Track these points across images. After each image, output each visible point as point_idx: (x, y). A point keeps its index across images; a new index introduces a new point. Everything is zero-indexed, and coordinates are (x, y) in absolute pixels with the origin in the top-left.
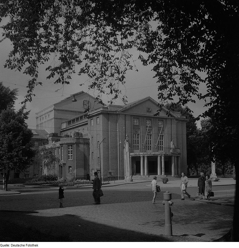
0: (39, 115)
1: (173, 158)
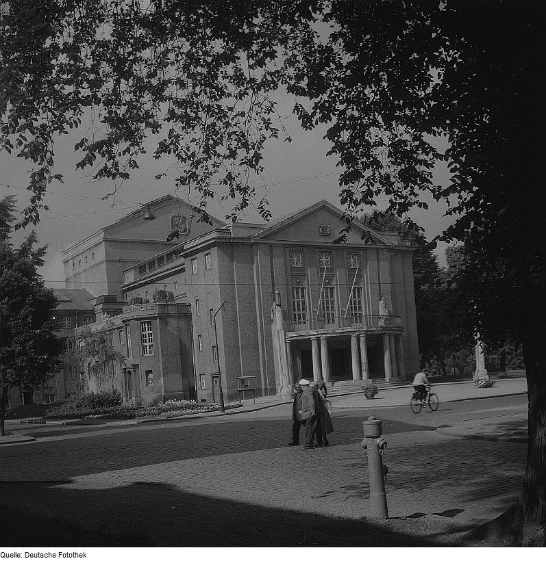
0: (70, 255)
1: (387, 338)
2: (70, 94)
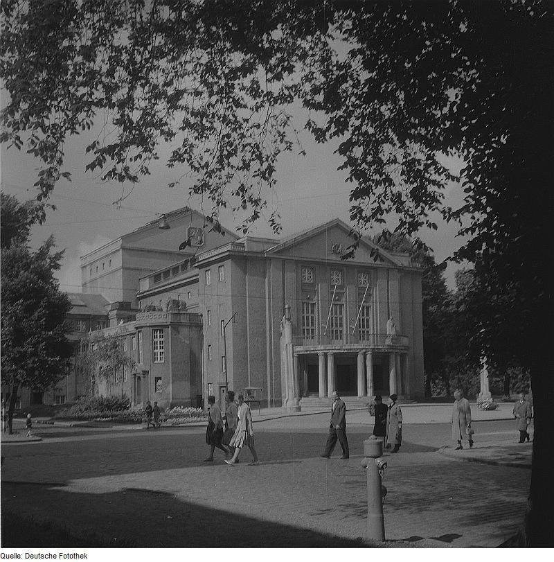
0: (88, 260)
1: (393, 357)
2: (84, 95)
